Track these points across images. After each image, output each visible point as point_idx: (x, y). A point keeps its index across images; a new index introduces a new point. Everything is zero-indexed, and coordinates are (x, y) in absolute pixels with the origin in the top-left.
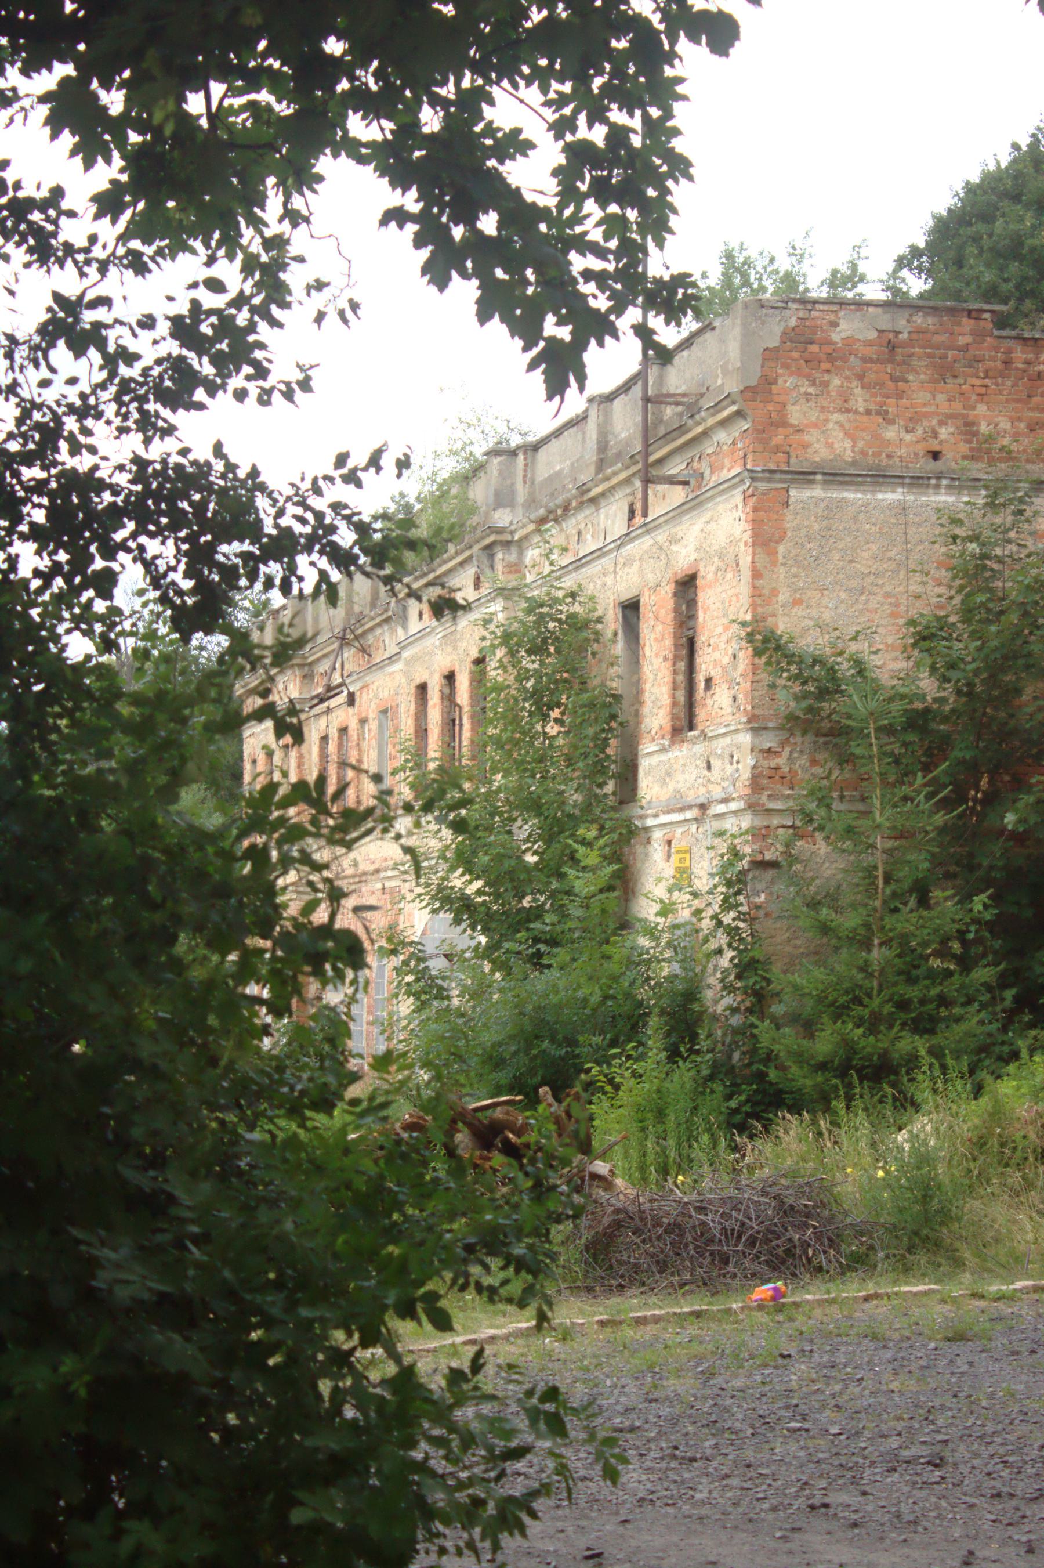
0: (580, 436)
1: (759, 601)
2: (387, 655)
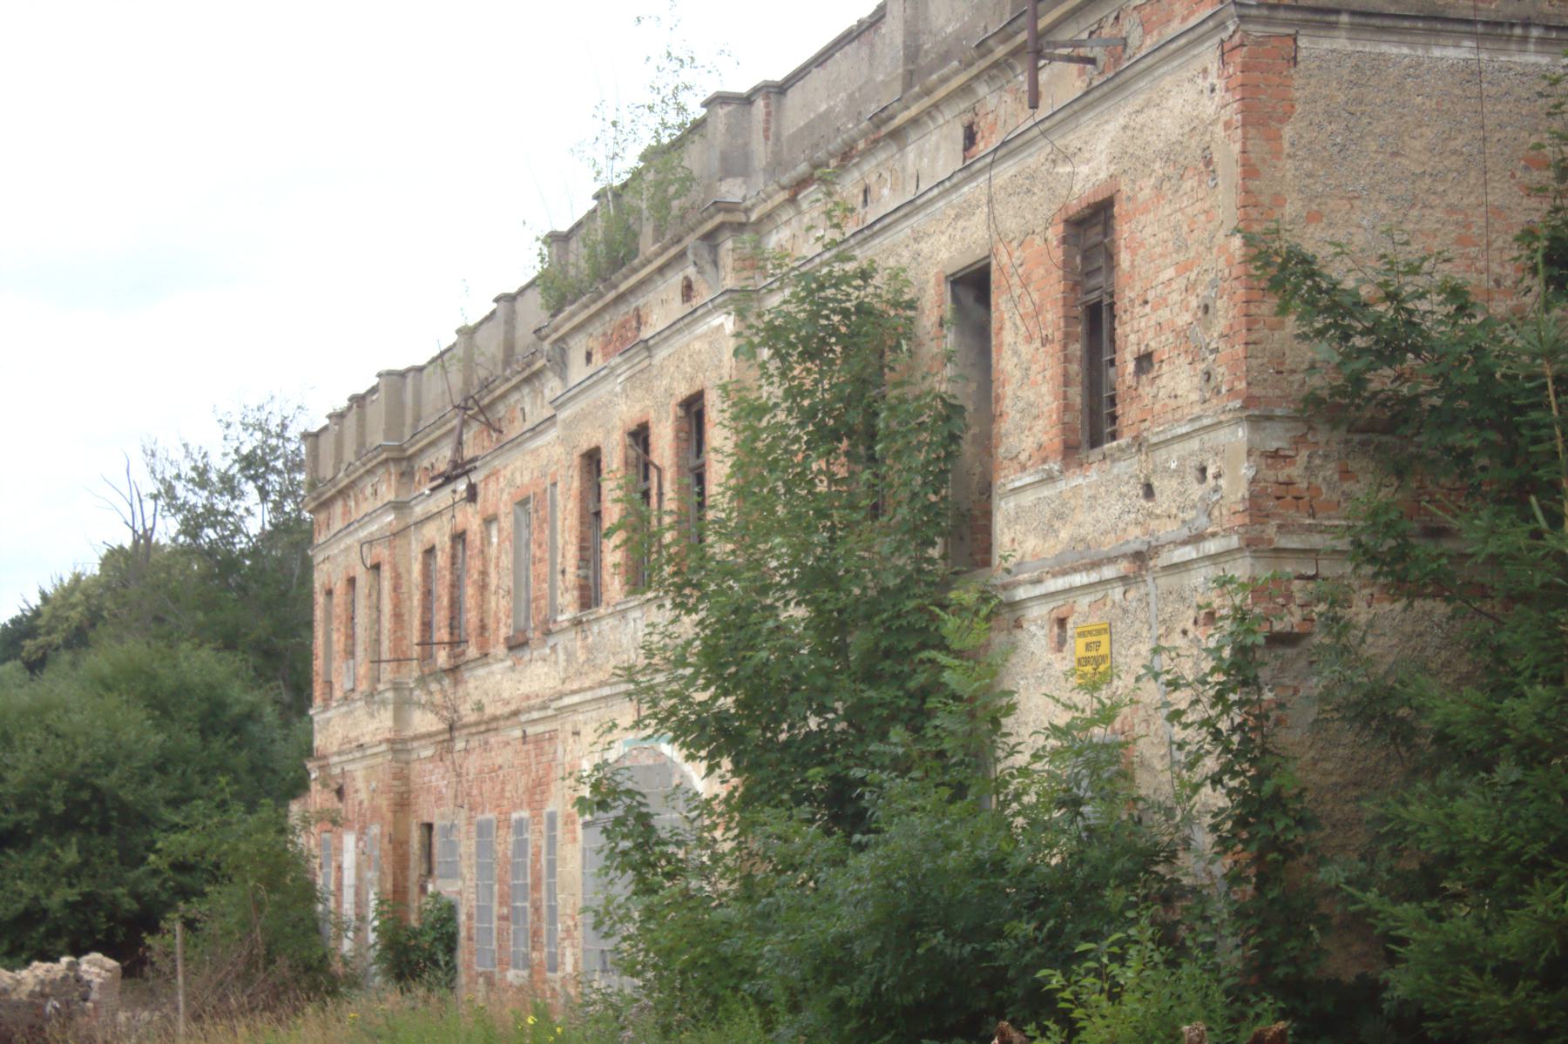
0: (865, 52)
1: (1254, 213)
2: (528, 425)
